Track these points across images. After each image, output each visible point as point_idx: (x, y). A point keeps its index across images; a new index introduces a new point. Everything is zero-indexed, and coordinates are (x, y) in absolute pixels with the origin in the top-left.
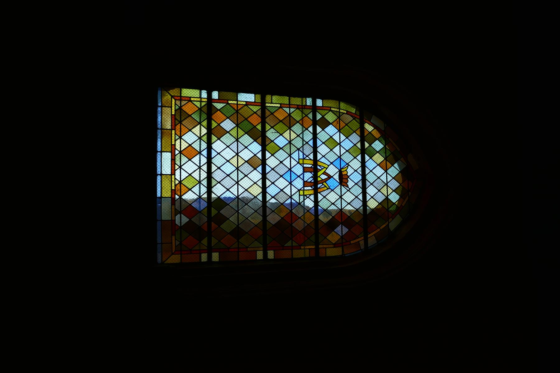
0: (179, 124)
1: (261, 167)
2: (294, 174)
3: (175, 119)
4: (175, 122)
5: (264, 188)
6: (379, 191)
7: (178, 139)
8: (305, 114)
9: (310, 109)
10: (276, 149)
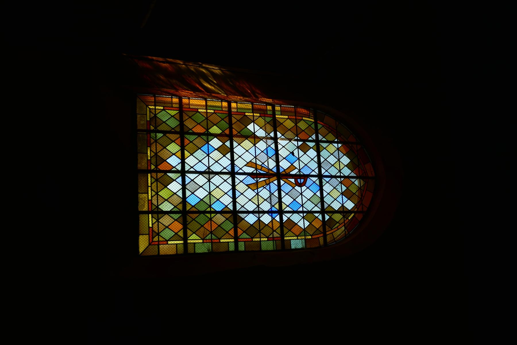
0: (157, 236)
1: (229, 153)
2: (261, 198)
3: (152, 203)
4: (152, 234)
5: (234, 198)
6: (335, 188)
7: (154, 195)
8: (267, 133)
9: (271, 117)
10: (248, 231)
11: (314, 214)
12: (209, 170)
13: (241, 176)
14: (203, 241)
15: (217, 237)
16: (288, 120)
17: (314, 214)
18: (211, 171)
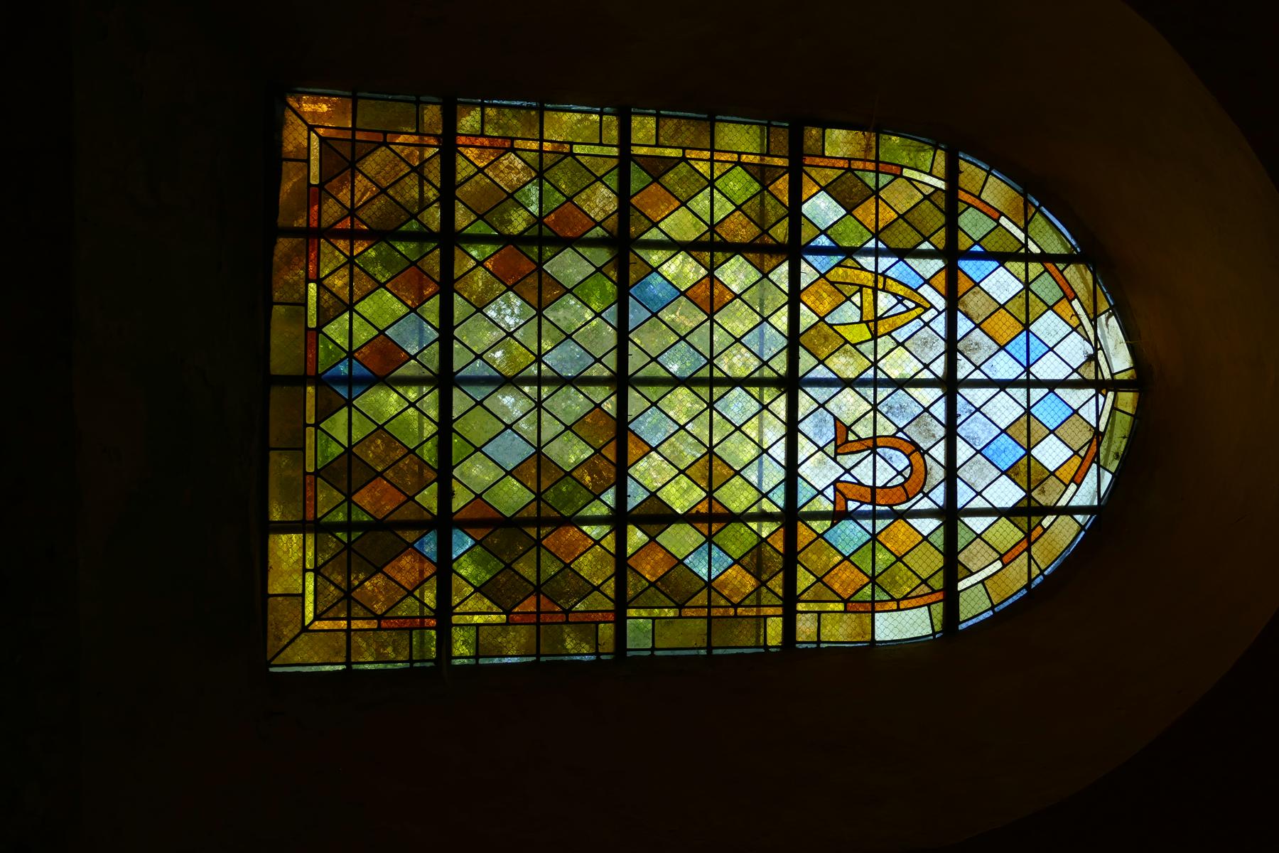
11: (399, 533)
12: (875, 373)
13: (928, 390)
14: (845, 607)
15: (853, 602)
16: (739, 168)
17: (399, 533)
18: (1034, 378)
